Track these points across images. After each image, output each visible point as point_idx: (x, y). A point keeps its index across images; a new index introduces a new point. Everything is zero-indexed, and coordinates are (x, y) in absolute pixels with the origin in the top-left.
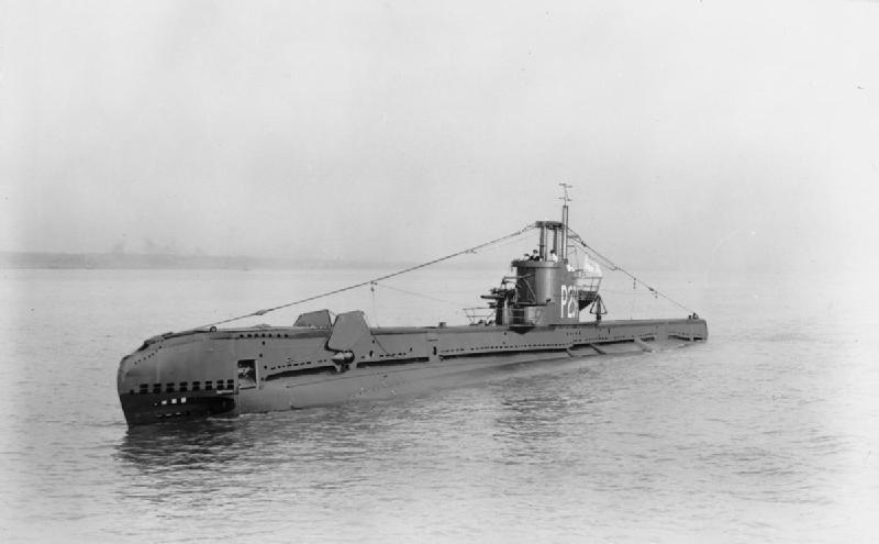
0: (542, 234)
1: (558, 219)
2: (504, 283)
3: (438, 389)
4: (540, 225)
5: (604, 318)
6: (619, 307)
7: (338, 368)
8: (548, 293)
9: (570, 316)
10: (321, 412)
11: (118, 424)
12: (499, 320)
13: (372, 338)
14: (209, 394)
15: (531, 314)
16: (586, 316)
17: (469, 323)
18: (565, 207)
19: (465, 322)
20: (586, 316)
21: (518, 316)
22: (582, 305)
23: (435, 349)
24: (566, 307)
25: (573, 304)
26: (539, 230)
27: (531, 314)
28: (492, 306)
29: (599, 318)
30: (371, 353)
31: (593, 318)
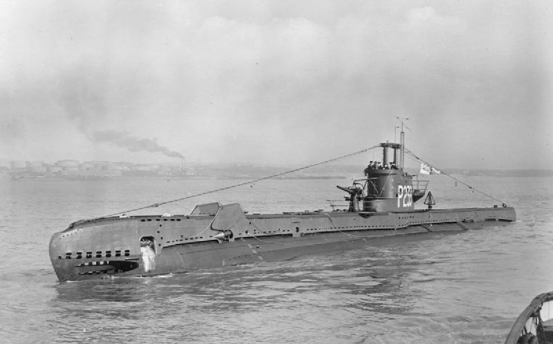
0: (384, 150)
1: (398, 142)
2: (355, 184)
3: (296, 257)
4: (384, 145)
5: (434, 207)
6: (54, 289)
7: (220, 241)
8: (391, 195)
9: (405, 205)
10: (75, 313)
11: (50, 273)
12: (352, 210)
13: (248, 221)
14: (119, 259)
15: (378, 205)
16: (420, 205)
17: (332, 210)
18: (402, 133)
19: (328, 209)
20: (420, 205)
21: (368, 207)
22: (415, 198)
23: (297, 228)
24: (401, 200)
25: (407, 197)
26: (383, 148)
27: (378, 205)
28: (347, 199)
29: (430, 207)
30: (247, 232)
31: (426, 207)
